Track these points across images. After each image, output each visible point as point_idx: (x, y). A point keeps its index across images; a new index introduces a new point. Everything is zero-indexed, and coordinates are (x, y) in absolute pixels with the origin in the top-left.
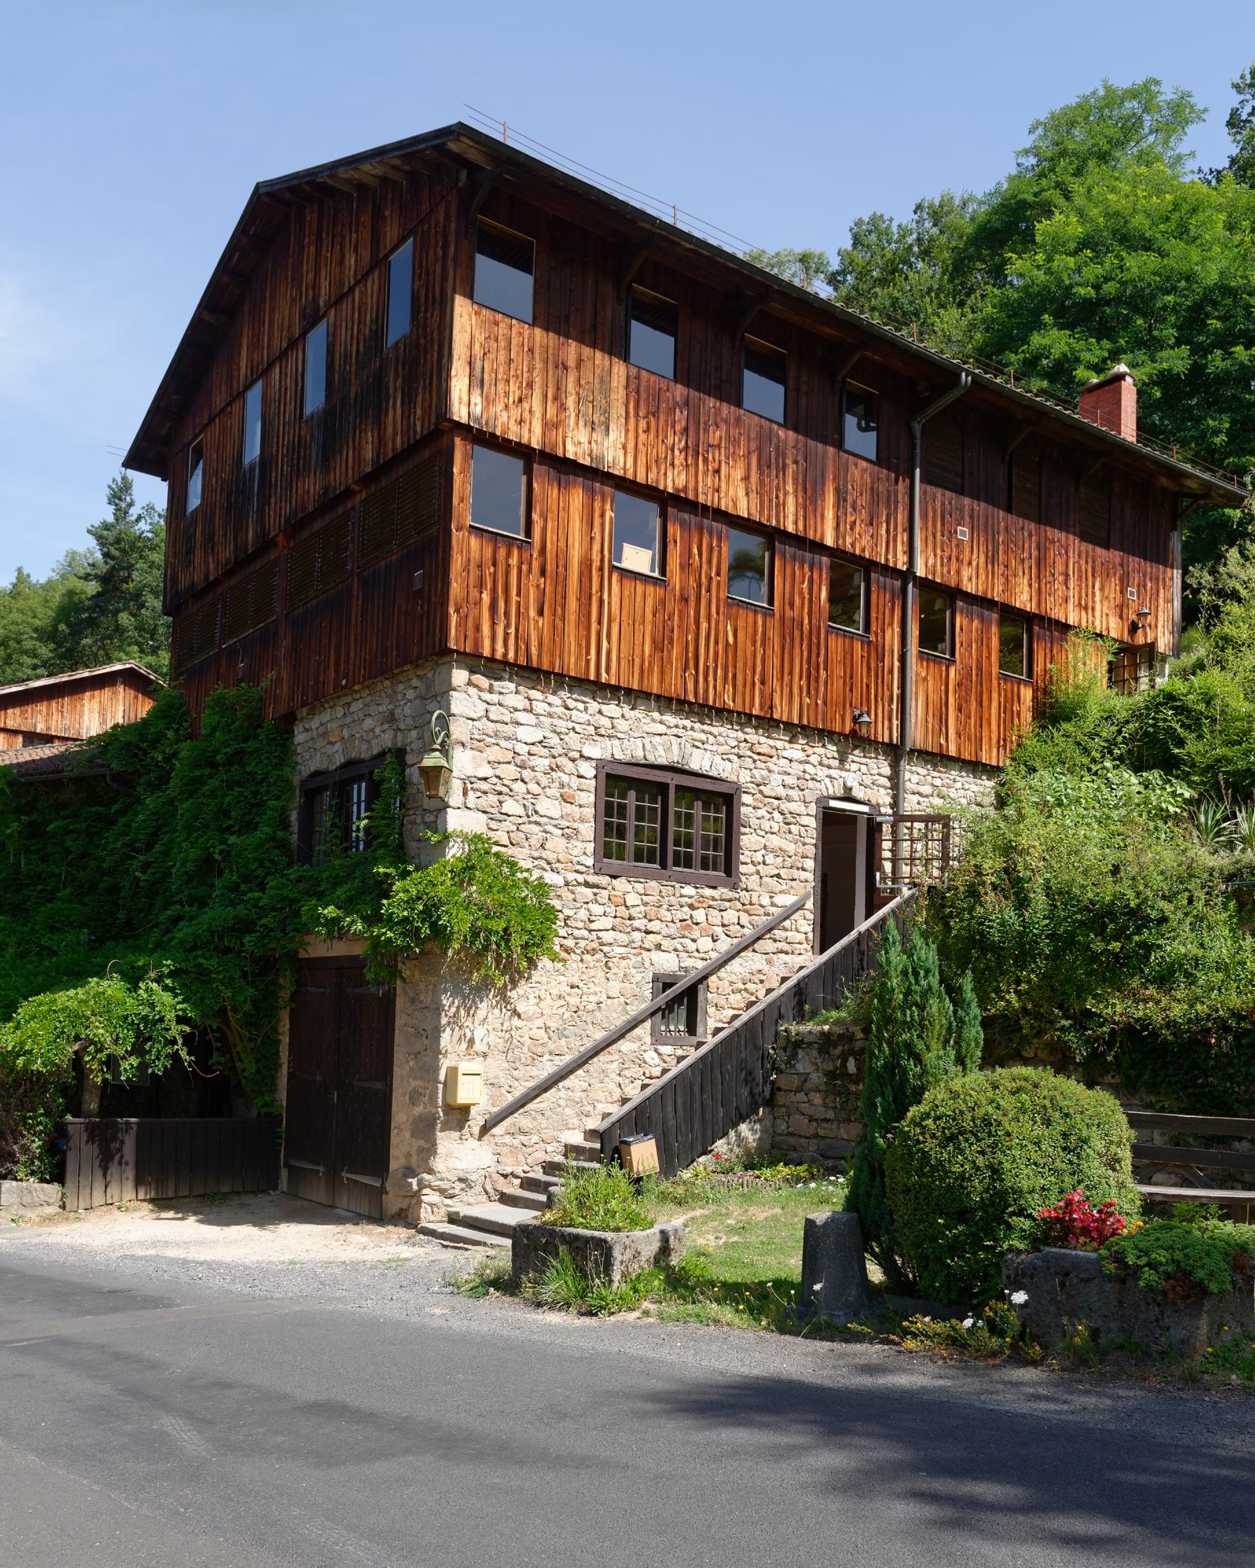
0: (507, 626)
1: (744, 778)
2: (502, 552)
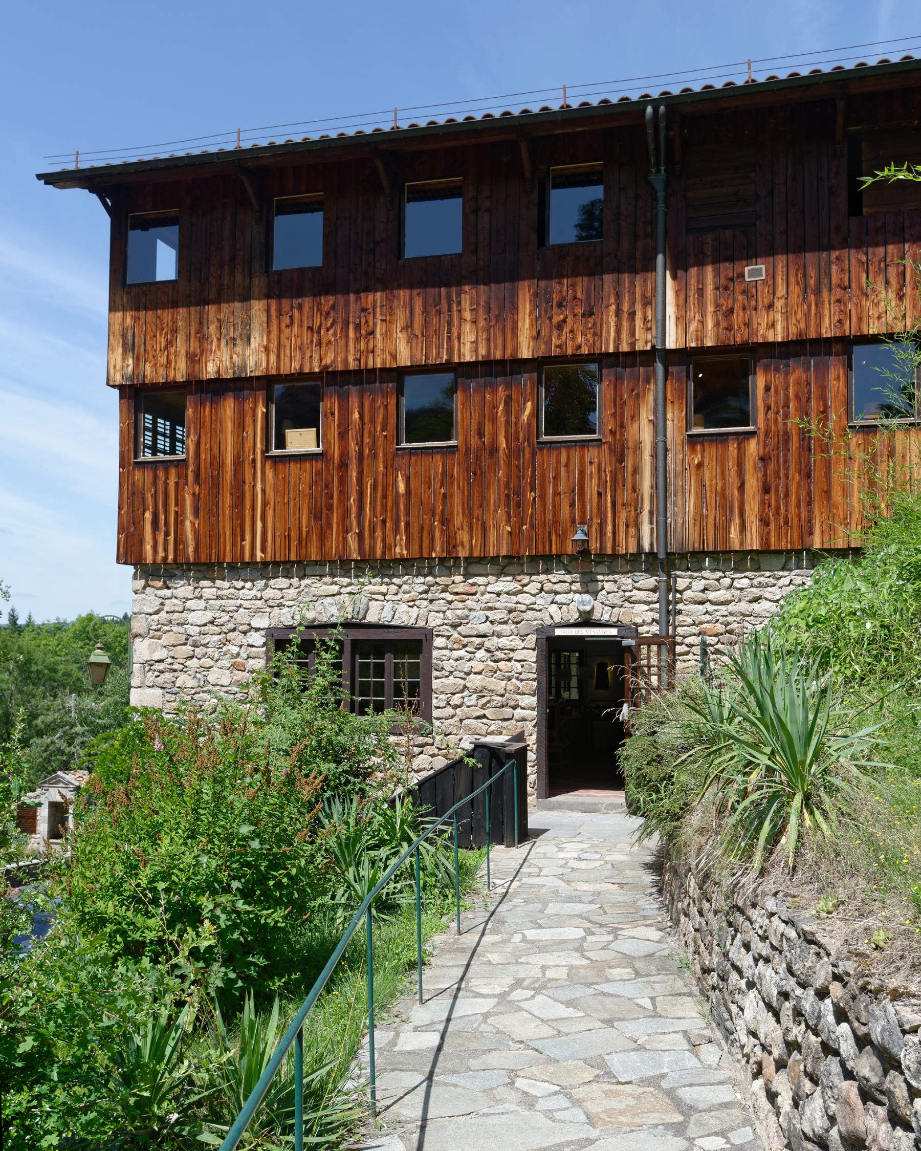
0: (167, 534)
1: (435, 621)
2: (161, 474)
